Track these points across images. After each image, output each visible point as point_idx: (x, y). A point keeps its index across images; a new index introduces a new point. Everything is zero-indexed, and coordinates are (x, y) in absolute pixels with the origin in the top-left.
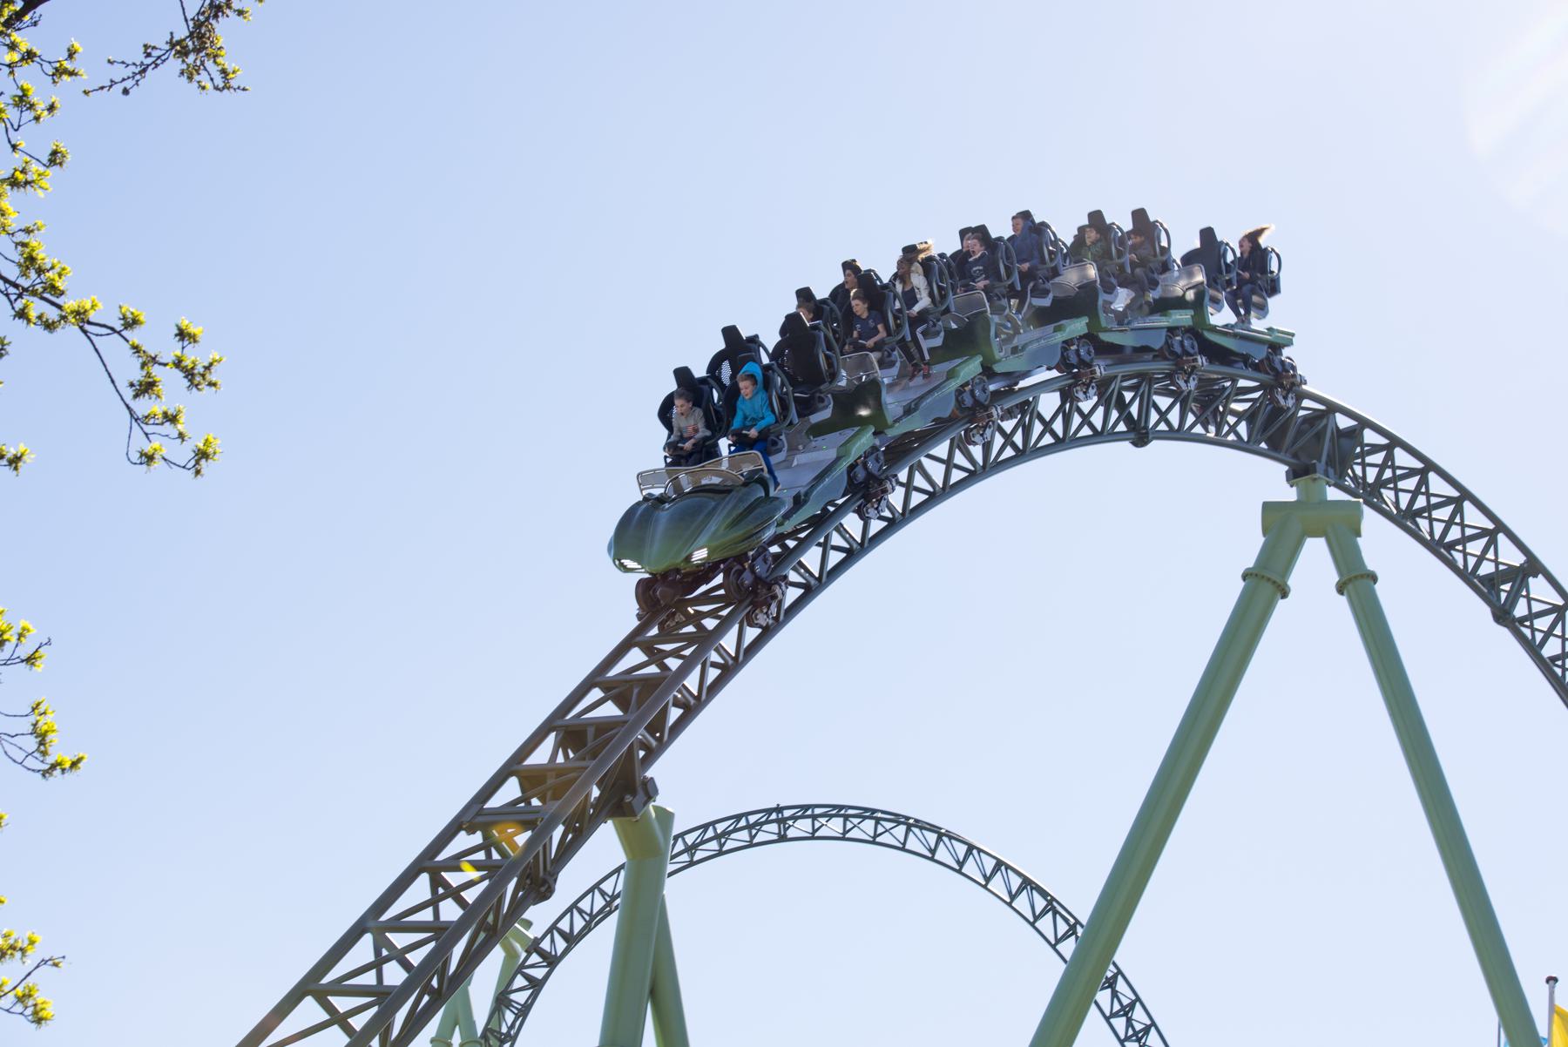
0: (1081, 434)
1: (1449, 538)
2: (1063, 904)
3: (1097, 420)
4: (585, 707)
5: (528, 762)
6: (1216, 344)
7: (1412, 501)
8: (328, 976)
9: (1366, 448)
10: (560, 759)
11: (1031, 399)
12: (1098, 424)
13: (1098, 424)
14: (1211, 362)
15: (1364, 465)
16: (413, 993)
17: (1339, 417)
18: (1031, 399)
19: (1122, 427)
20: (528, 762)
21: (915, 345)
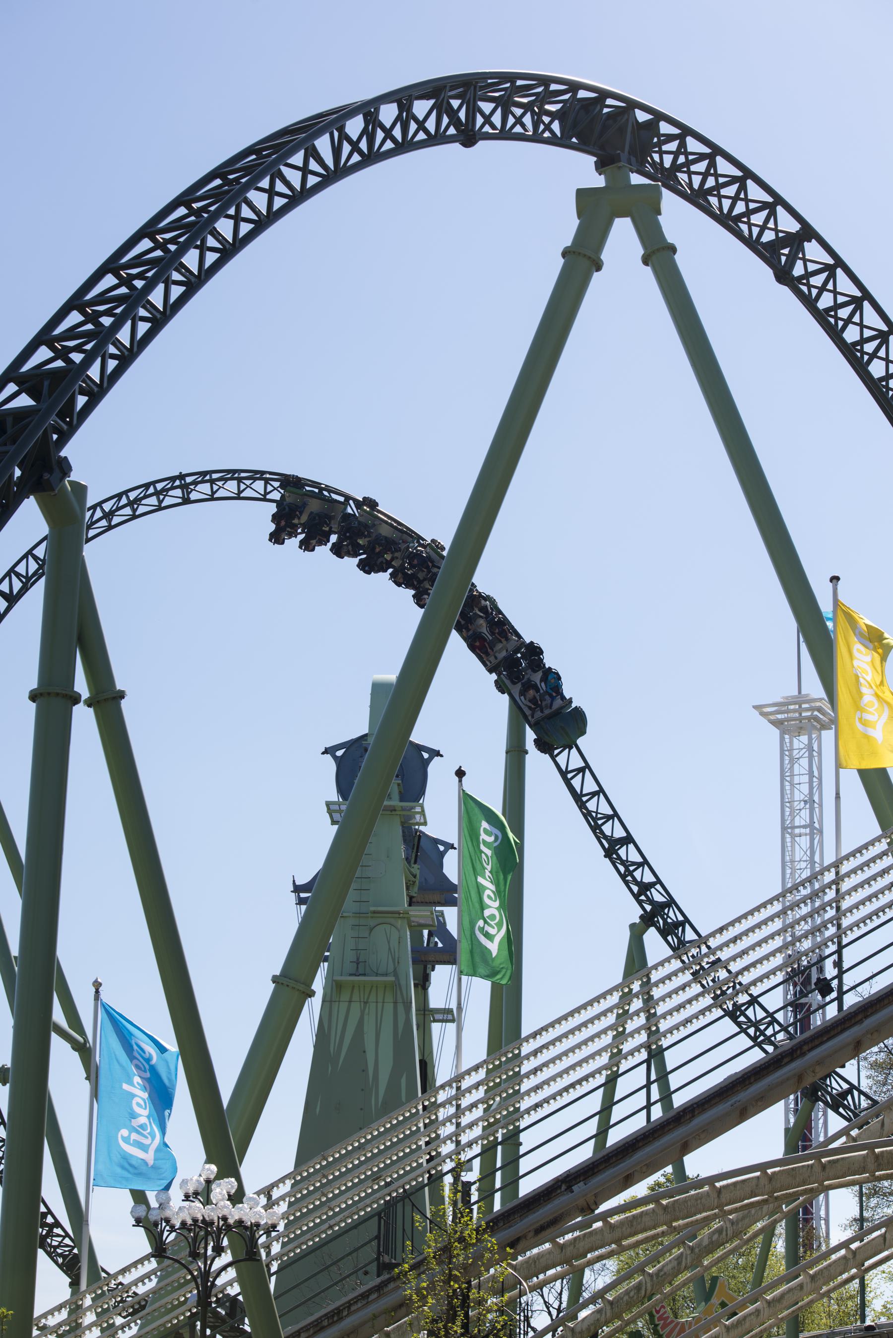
1: (707, 186)
7: (703, 182)
9: (715, 193)
11: (372, 110)
18: (372, 110)
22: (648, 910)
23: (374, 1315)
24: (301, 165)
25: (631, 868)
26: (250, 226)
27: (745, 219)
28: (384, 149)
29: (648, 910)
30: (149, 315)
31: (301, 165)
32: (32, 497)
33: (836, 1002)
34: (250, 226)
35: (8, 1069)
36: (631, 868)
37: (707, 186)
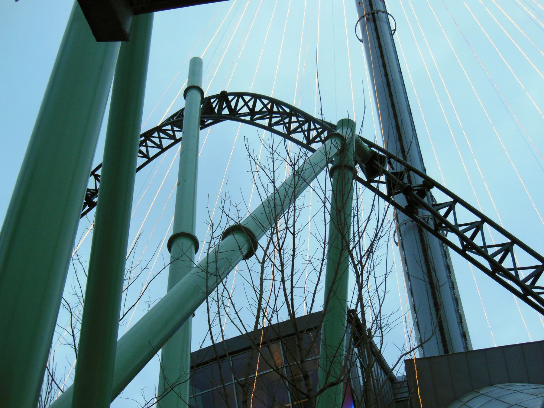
0: (233, 97)
1: (307, 125)
2: (246, 328)
3: (241, 103)
4: (540, 290)
5: (510, 271)
6: (540, 304)
7: (309, 126)
8: (236, 101)
9: (301, 123)
10: (445, 232)
11: (420, 205)
12: (241, 101)
13: (241, 101)
14: (98, 193)
15: (298, 121)
16: (541, 304)
17: (435, 191)
18: (420, 205)
19: (230, 98)
20: (510, 271)
21: (436, 206)
22: (494, 258)
23: (48, 380)
24: (296, 120)
25: (468, 234)
26: (245, 97)
27: (319, 131)
28: (214, 99)
29: (494, 258)
30: (447, 208)
31: (296, 120)
32: (515, 244)
33: (536, 285)
34: (245, 97)
35: (423, 198)
36: (468, 234)
37: (307, 125)
